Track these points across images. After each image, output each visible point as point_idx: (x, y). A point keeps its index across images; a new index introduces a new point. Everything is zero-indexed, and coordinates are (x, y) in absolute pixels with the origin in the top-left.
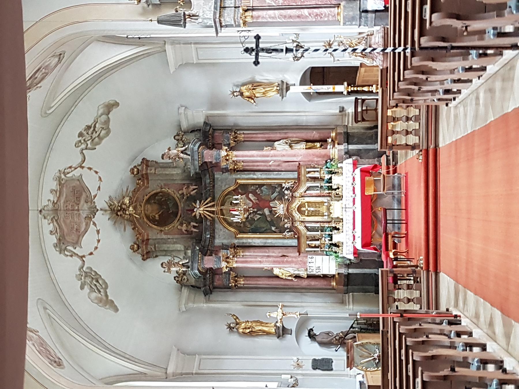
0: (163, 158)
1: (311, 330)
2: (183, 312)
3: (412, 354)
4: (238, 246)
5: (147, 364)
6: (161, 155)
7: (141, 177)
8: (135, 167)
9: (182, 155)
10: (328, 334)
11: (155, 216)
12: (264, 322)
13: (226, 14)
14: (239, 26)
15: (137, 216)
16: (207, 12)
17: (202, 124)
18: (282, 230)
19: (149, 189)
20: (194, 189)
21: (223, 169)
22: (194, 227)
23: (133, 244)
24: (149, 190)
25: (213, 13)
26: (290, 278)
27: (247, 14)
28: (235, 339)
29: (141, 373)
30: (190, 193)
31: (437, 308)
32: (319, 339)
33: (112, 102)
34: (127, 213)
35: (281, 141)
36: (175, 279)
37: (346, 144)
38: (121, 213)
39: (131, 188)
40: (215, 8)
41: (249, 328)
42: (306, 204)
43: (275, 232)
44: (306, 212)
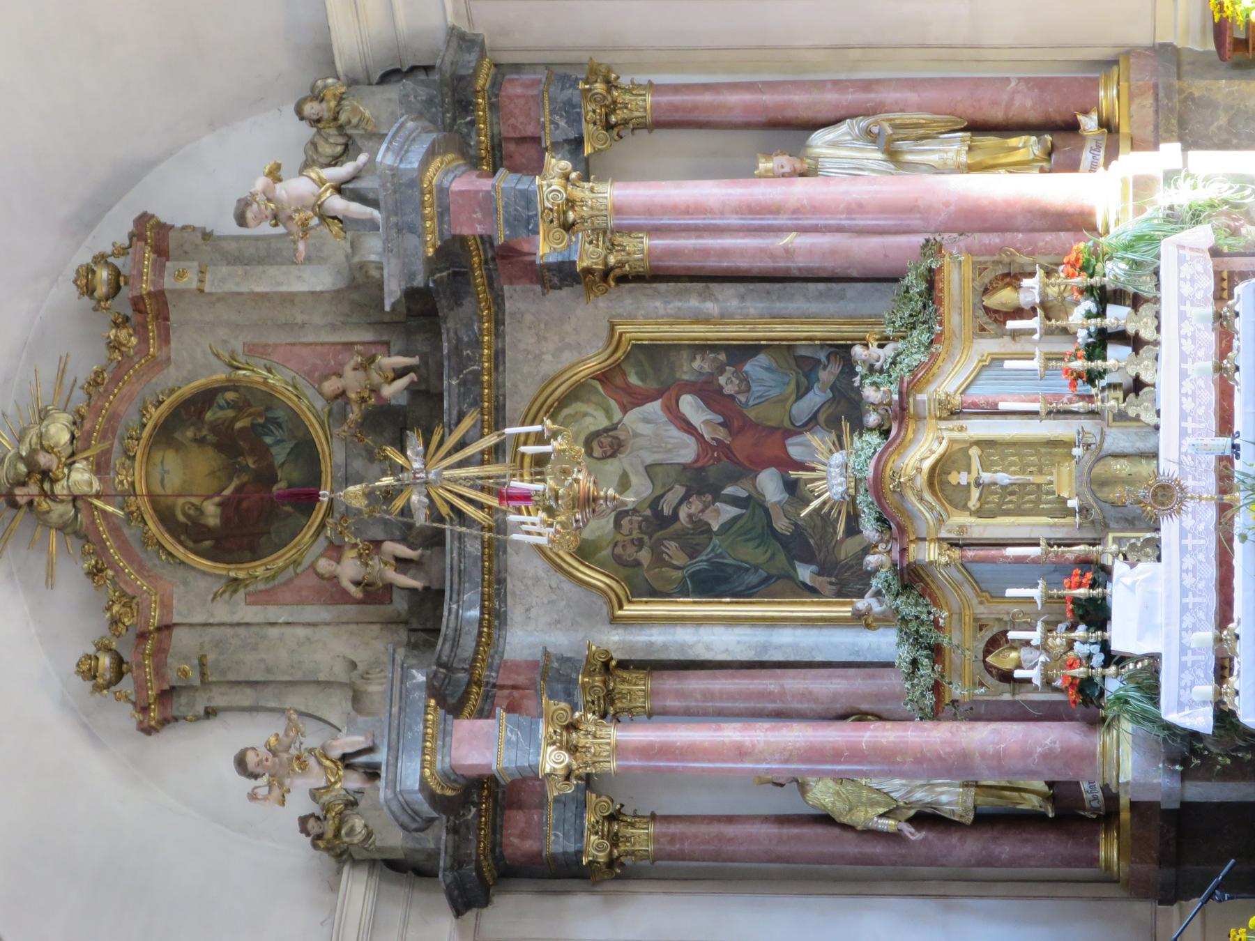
0: (241, 220)
4: (624, 665)
6: (231, 207)
7: (129, 312)
8: (101, 259)
9: (338, 204)
11: (199, 510)
15: (110, 509)
17: (441, 36)
18: (848, 580)
19: (172, 369)
20: (400, 373)
21: (549, 267)
22: (402, 564)
23: (91, 650)
24: (172, 375)
26: (888, 824)
30: (375, 390)
34: (59, 489)
35: (844, 127)
36: (304, 829)
37: (1177, 146)
38: (33, 489)
39: (86, 362)
42: (974, 452)
43: (813, 591)
44: (975, 493)
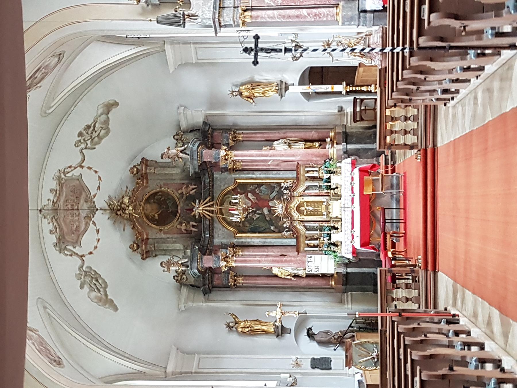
0: (162, 158)
1: (310, 329)
2: (182, 311)
3: (411, 353)
4: (237, 246)
5: (146, 363)
6: (160, 155)
7: (140, 177)
8: (135, 166)
9: (181, 155)
10: (326, 333)
11: (154, 216)
12: (263, 321)
13: (225, 14)
14: (238, 26)
15: (136, 216)
16: (206, 12)
17: (202, 124)
18: (281, 230)
19: (149, 188)
20: (193, 189)
21: (222, 168)
22: (194, 226)
23: (132, 243)
24: (149, 189)
25: (212, 12)
26: (289, 277)
27: (246, 14)
28: (234, 338)
29: (141, 372)
30: (189, 193)
31: (435, 307)
32: (317, 338)
33: (111, 102)
34: (127, 212)
35: (280, 141)
36: (174, 279)
37: (345, 143)
38: (121, 212)
39: (131, 188)
40: (215, 8)
41: (248, 327)
42: (305, 203)
43: (274, 232)
44: (305, 211)
